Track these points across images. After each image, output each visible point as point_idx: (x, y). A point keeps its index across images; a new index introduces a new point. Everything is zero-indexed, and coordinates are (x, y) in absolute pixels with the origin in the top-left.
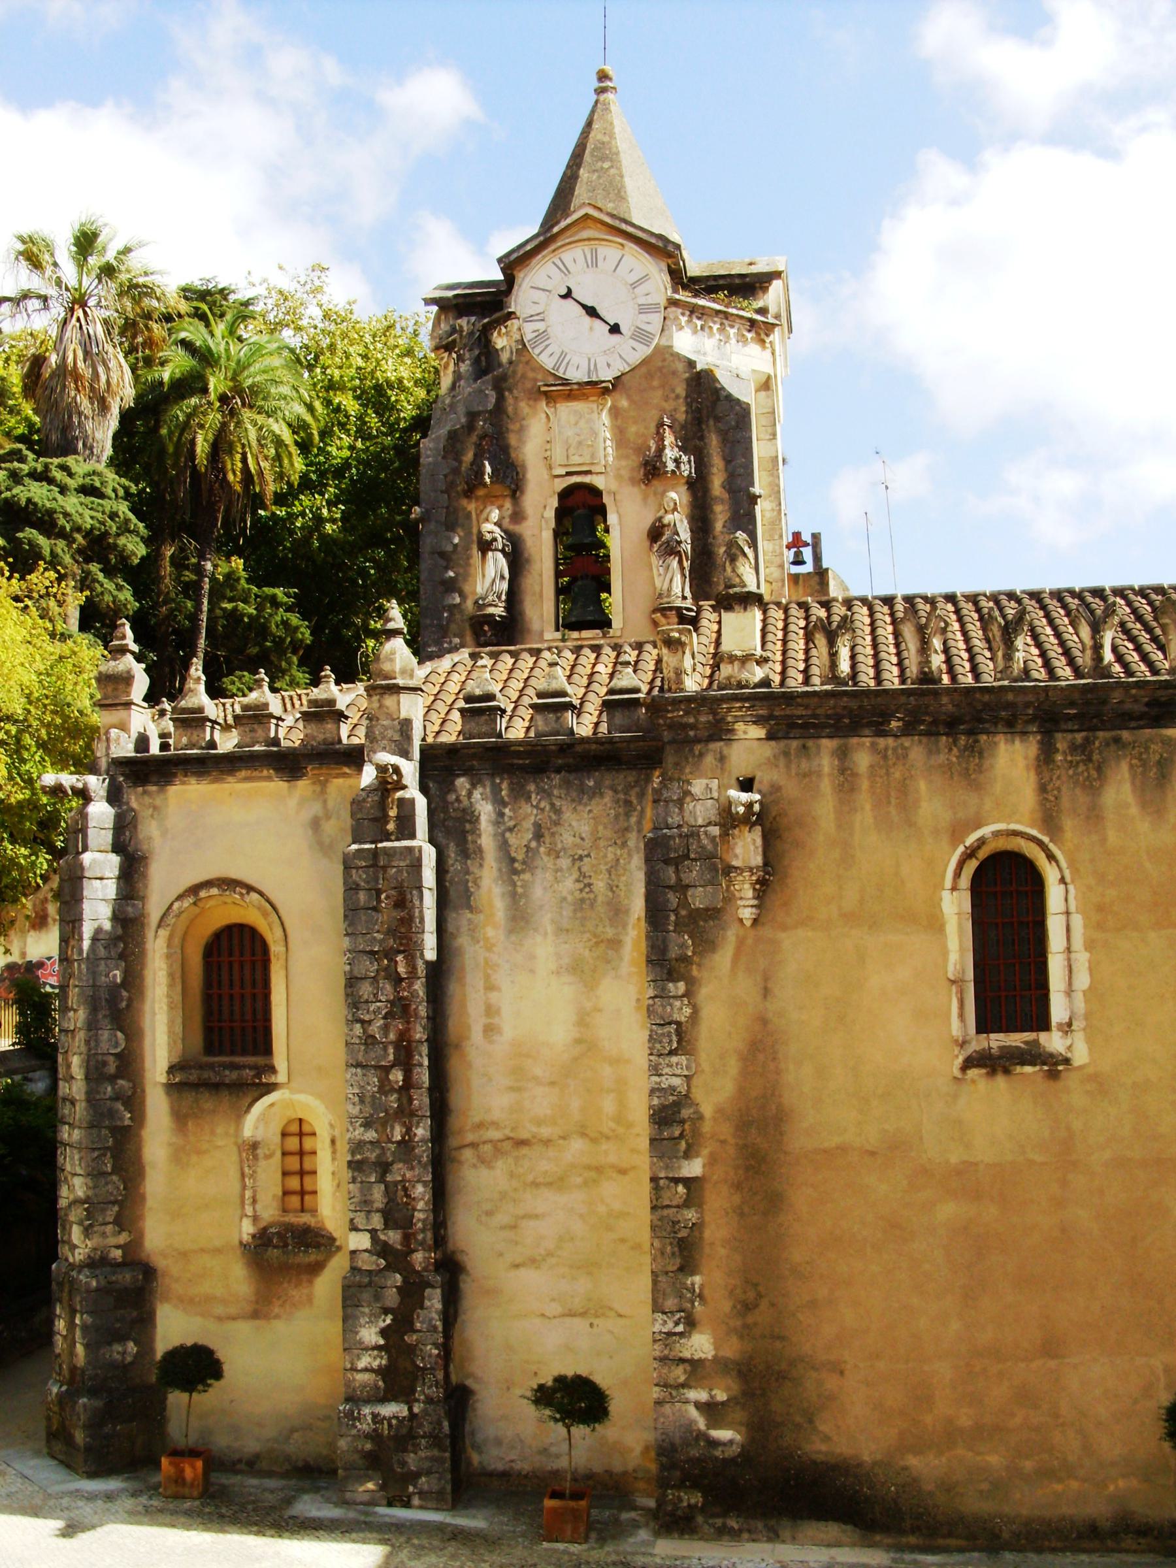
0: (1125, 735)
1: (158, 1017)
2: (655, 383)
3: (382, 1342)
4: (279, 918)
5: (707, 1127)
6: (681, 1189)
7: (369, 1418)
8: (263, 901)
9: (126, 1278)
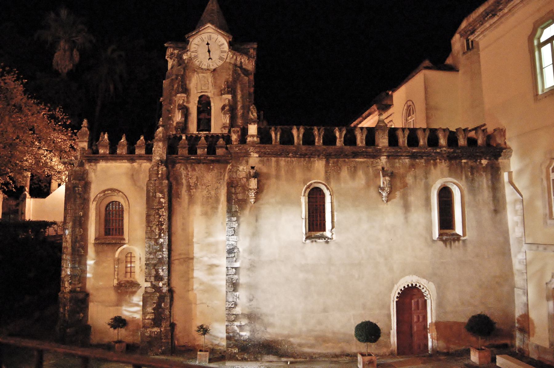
0: (346, 160)
1: (92, 225)
3: (153, 311)
4: (127, 199)
5: (241, 254)
6: (234, 270)
8: (123, 195)
9: (81, 296)
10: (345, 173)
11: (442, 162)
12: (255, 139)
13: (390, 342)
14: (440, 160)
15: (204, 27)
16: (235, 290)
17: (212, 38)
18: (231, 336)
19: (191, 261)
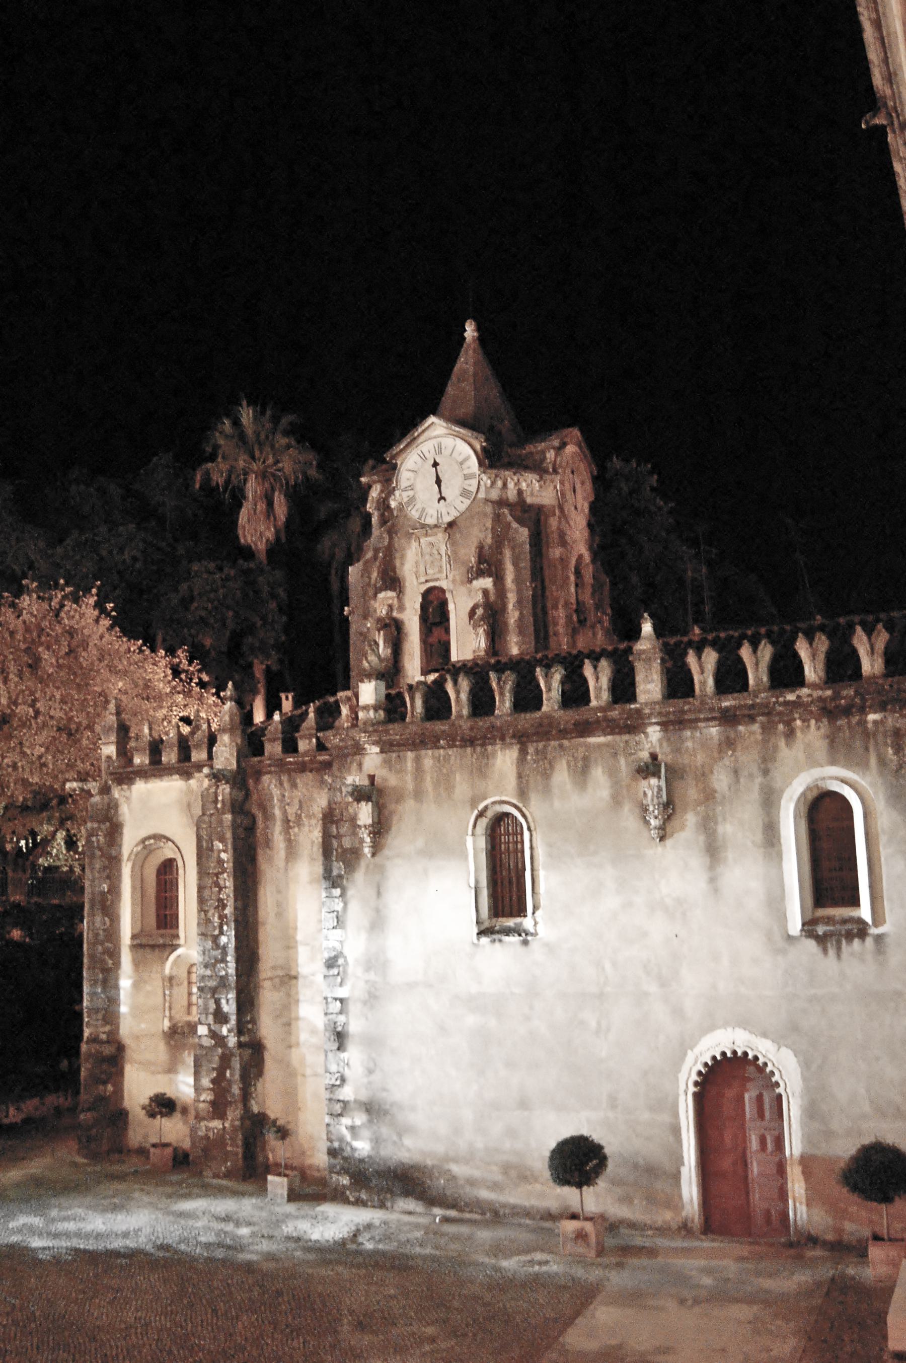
0: (566, 743)
2: (475, 522)
5: (350, 969)
6: (338, 1003)
7: (204, 1128)
9: (107, 1050)
10: (561, 775)
11: (808, 726)
12: (372, 713)
13: (680, 1196)
14: (804, 721)
15: (423, 428)
16: (341, 1048)
17: (443, 447)
18: (335, 1149)
19: (294, 981)
